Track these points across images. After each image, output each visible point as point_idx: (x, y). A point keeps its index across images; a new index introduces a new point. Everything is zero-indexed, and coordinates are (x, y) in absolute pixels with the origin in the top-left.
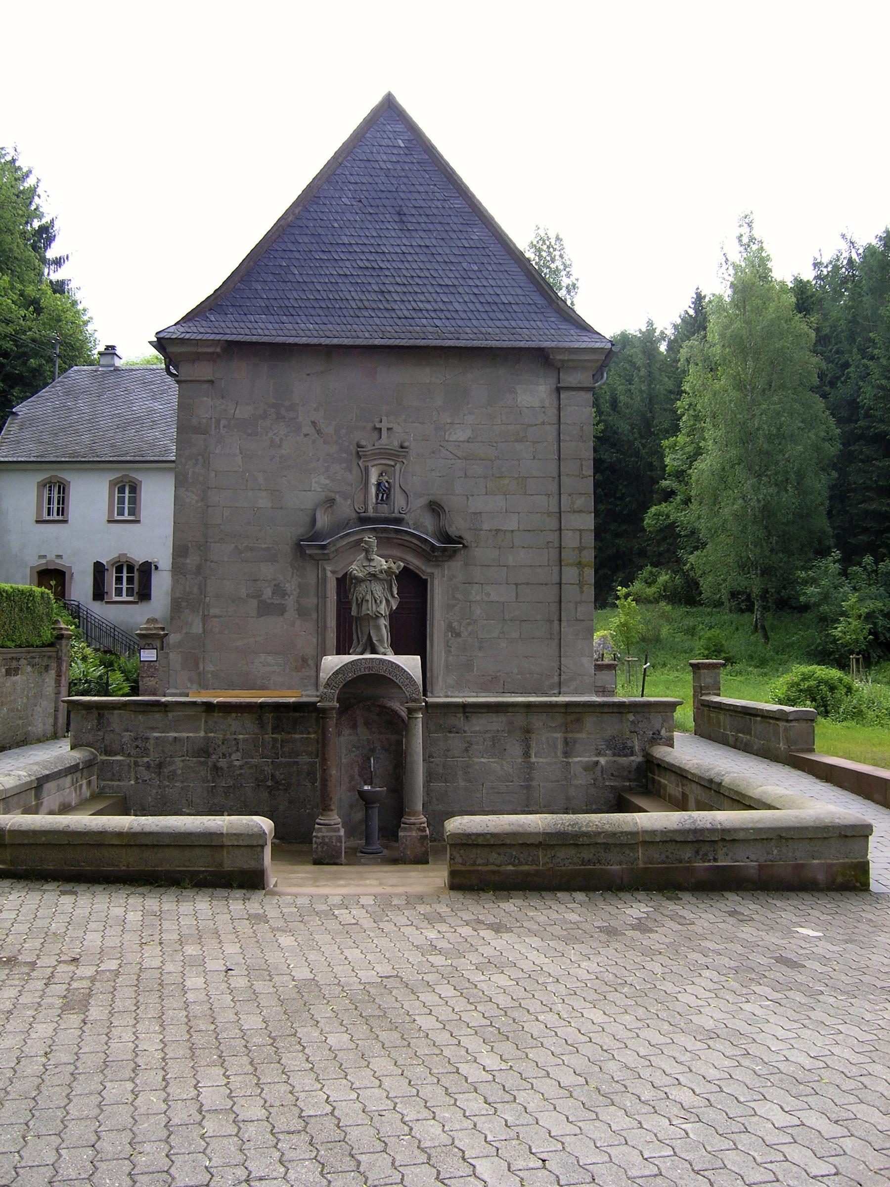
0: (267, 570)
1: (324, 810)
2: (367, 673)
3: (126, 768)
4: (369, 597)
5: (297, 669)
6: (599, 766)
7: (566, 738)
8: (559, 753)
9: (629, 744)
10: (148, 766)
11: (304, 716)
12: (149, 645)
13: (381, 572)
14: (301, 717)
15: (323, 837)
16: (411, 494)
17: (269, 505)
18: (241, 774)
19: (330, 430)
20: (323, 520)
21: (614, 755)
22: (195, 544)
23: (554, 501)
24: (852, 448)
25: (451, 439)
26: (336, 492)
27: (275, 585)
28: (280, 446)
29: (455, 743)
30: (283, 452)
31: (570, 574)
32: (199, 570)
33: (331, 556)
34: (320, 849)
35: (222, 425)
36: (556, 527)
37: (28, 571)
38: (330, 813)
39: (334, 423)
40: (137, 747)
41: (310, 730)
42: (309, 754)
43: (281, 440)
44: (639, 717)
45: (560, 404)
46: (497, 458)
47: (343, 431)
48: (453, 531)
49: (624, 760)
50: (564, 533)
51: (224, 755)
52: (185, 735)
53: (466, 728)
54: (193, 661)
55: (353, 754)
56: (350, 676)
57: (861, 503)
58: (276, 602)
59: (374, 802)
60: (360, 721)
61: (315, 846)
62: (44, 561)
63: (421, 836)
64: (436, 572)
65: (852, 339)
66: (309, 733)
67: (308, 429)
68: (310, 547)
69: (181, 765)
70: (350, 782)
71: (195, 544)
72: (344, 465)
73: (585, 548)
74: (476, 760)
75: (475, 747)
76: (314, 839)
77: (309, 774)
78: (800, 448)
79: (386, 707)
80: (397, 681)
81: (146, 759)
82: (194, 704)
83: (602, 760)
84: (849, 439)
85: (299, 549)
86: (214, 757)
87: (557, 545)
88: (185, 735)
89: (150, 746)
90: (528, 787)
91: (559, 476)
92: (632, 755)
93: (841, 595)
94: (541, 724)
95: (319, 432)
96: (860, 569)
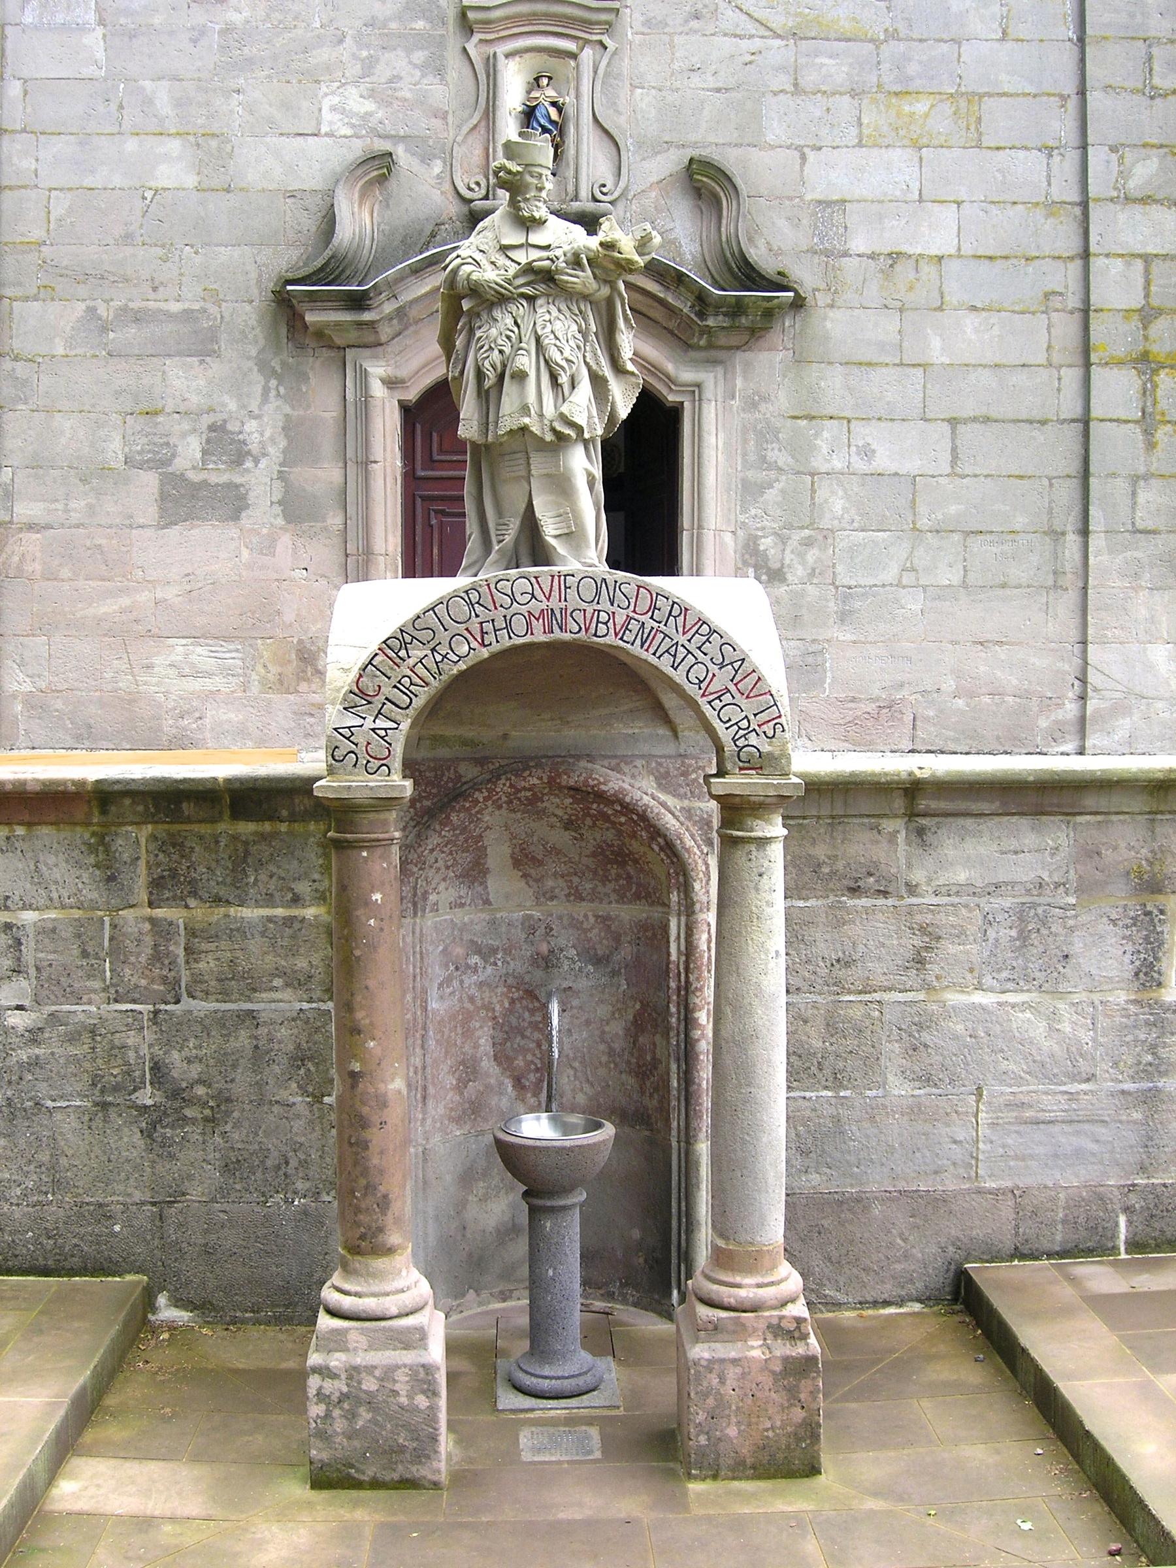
0: (185, 382)
1: (355, 1250)
2: (540, 637)
4: (526, 362)
5: (282, 685)
11: (275, 835)
13: (575, 262)
14: (263, 837)
15: (354, 1372)
17: (191, 181)
18: (35, 1063)
20: (357, 223)
23: (1066, 166)
27: (212, 428)
29: (876, 932)
31: (1116, 391)
33: (385, 331)
34: (339, 1425)
36: (1075, 246)
38: (380, 1263)
41: (303, 888)
42: (297, 982)
46: (893, 35)
48: (760, 256)
50: (1096, 264)
53: (918, 876)
55: (470, 980)
56: (465, 653)
58: (214, 479)
59: (567, 1190)
60: (498, 853)
61: (316, 1410)
63: (786, 1360)
64: (710, 379)
66: (296, 900)
68: (318, 306)
72: (419, 56)
73: (1160, 312)
74: (954, 998)
75: (953, 949)
76: (314, 1382)
77: (299, 1059)
79: (600, 796)
80: (678, 676)
85: (287, 309)
87: (1074, 302)
91: (1082, 93)
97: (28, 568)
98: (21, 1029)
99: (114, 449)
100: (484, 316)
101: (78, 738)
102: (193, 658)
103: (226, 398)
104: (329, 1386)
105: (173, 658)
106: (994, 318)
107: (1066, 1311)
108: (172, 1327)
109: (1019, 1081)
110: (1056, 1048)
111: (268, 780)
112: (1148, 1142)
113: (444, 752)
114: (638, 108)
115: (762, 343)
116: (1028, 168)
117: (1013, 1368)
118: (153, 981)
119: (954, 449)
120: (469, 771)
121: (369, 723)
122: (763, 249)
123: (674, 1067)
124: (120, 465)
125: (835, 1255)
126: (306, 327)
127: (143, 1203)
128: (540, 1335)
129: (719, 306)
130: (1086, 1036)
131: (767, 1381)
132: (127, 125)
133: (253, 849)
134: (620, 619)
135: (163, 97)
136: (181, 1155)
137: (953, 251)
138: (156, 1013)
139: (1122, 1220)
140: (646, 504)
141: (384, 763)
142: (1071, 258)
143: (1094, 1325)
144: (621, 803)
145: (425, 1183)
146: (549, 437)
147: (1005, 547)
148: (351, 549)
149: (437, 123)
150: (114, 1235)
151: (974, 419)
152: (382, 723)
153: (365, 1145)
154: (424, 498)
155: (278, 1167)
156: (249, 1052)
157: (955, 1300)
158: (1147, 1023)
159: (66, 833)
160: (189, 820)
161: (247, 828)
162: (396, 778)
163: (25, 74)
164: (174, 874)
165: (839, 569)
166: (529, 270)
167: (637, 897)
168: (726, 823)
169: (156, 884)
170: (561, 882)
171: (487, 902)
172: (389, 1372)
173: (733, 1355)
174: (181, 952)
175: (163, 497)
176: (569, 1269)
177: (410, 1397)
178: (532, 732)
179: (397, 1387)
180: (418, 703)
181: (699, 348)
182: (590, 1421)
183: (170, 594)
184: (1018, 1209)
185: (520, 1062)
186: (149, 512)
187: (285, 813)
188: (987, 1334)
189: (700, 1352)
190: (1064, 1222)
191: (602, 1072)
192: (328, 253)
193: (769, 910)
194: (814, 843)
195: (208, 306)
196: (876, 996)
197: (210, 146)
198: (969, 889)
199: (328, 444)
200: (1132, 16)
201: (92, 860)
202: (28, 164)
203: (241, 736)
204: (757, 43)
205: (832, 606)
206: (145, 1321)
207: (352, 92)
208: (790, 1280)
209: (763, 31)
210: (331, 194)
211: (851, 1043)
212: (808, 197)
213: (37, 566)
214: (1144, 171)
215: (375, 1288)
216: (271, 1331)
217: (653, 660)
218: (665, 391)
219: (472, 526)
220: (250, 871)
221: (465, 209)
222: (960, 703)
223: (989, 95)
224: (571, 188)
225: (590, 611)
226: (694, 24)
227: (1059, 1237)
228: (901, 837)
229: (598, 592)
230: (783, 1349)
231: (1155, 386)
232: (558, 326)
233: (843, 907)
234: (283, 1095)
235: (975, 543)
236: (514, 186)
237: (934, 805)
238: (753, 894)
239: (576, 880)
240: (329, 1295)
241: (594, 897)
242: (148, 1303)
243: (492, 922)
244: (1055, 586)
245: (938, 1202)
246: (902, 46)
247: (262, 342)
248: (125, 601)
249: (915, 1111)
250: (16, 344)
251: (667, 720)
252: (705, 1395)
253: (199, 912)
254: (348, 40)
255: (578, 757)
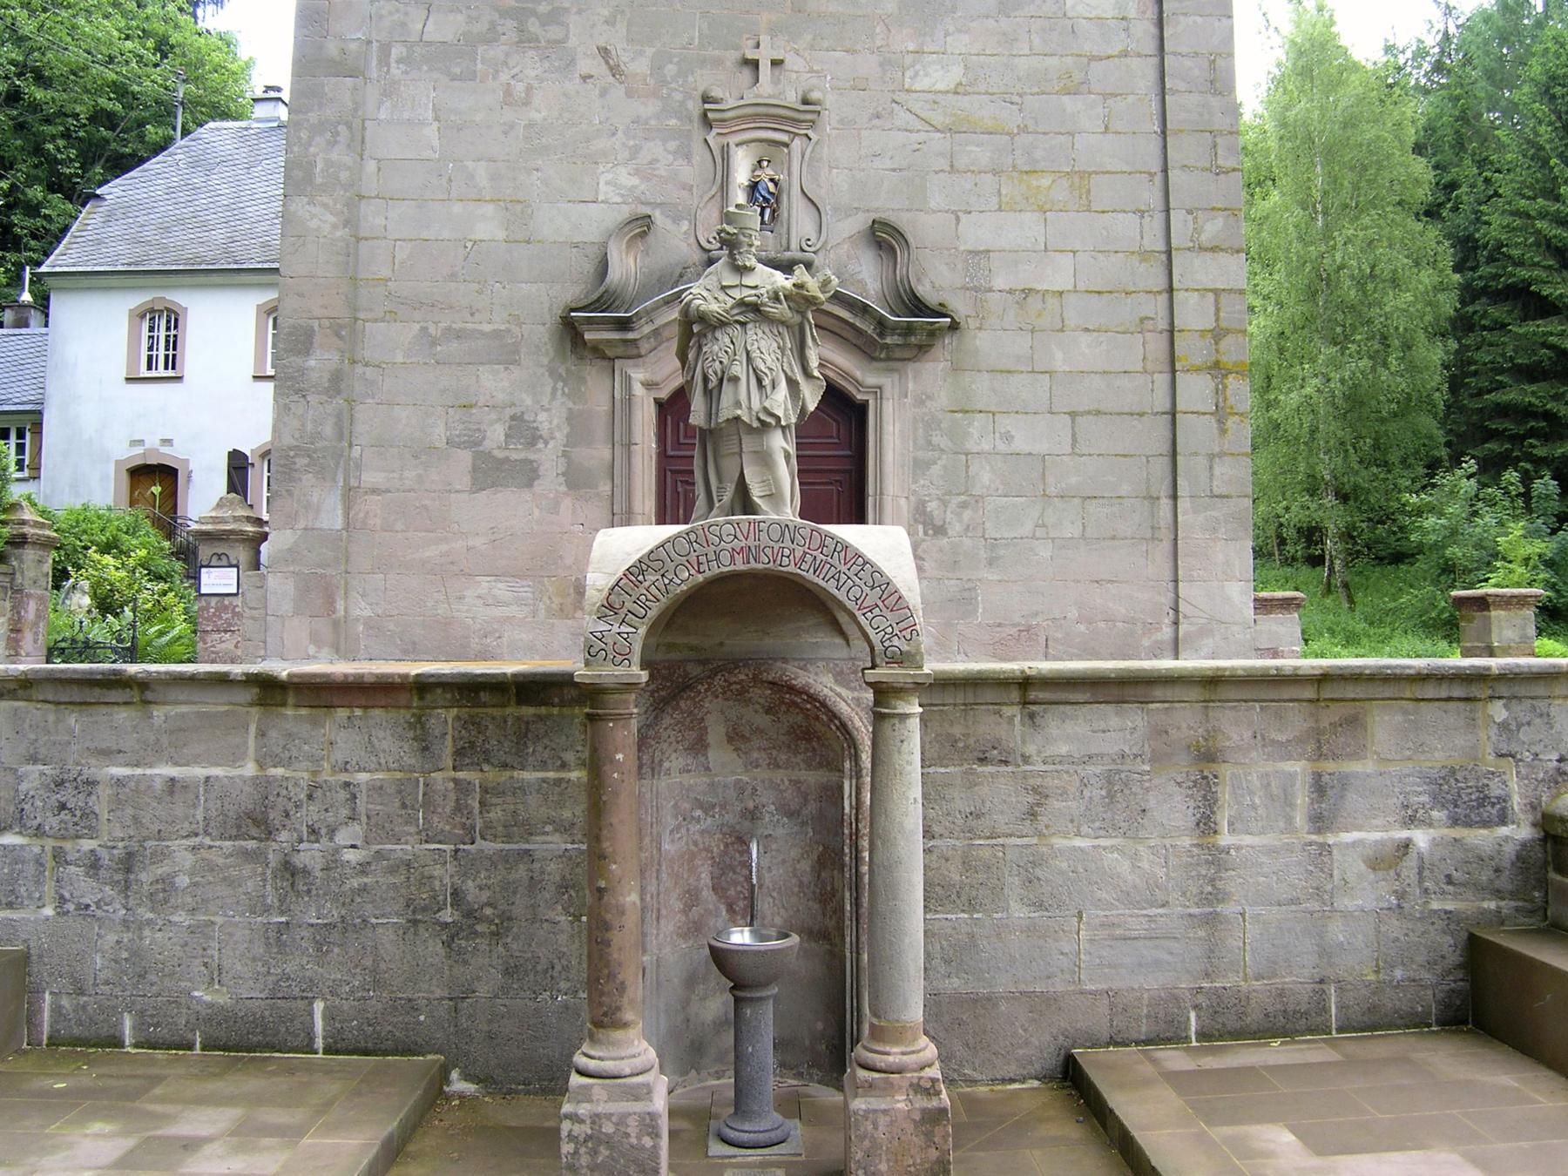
0: (494, 383)
1: (599, 1024)
2: (740, 566)
3: (31, 869)
4: (739, 369)
5: (562, 612)
6: (1413, 854)
7: (1318, 776)
8: (1300, 819)
9: (1495, 790)
10: (93, 865)
12: (219, 556)
13: (776, 298)
14: (540, 718)
15: (596, 1118)
16: (826, 209)
18: (364, 889)
19: (639, 67)
20: (625, 267)
21: (1455, 822)
22: (326, 323)
24: (1470, 309)
25: (917, 87)
26: (655, 205)
27: (513, 418)
28: (526, 103)
29: (999, 791)
30: (537, 116)
31: (1195, 390)
32: (336, 382)
33: (644, 347)
34: (585, 1160)
35: (394, 56)
36: (1162, 283)
37: (112, 467)
38: (618, 1034)
39: (650, 51)
40: (63, 806)
41: (569, 757)
43: (529, 88)
44: (1521, 711)
45: (1161, 12)
46: (1023, 129)
47: (671, 69)
48: (925, 291)
49: (1480, 838)
50: (1179, 296)
51: (313, 831)
52: (199, 772)
53: (1030, 749)
54: (321, 594)
56: (686, 579)
57: (1489, 392)
58: (514, 456)
60: (716, 732)
61: (567, 1148)
62: (139, 450)
63: (924, 1111)
64: (887, 382)
65: (1460, 145)
66: (564, 766)
67: (589, 64)
68: (592, 330)
69: (188, 860)
70: (686, 910)
71: (326, 323)
72: (672, 145)
73: (1227, 332)
74: (1059, 842)
76: (566, 1126)
77: (563, 887)
78: (1409, 296)
79: (792, 689)
81: (87, 845)
82: (223, 680)
83: (1421, 838)
84: (1469, 294)
85: (571, 332)
86: (283, 836)
87: (1163, 324)
88: (199, 772)
89: (101, 803)
90: (1212, 921)
91: (1165, 170)
92: (1503, 820)
93: (1478, 530)
94: (1248, 734)
95: (615, 70)
96: (1499, 493)
97: (371, 522)
98: (354, 863)
99: (439, 434)
100: (709, 336)
101: (406, 652)
102: (496, 592)
103: (524, 396)
104: (578, 1129)
105: (480, 591)
106: (1103, 337)
107: (1147, 1083)
108: (461, 1096)
109: (1110, 906)
110: (1138, 881)
111: (545, 675)
112: (1210, 954)
113: (675, 656)
114: (834, 184)
115: (928, 356)
116: (1126, 225)
117: (1104, 1126)
118: (454, 827)
119: (1074, 435)
120: (695, 670)
121: (615, 629)
122: (928, 286)
123: (847, 895)
124: (443, 445)
125: (971, 1042)
126: (585, 343)
127: (443, 999)
128: (742, 1102)
129: (895, 328)
130: (1161, 872)
131: (910, 1127)
132: (454, 194)
133: (532, 727)
134: (798, 554)
135: (481, 172)
136: (472, 962)
137: (1070, 287)
138: (457, 851)
139: (1193, 1015)
140: (840, 472)
141: (626, 657)
142: (1159, 293)
143: (1168, 1093)
144: (810, 696)
145: (658, 984)
146: (756, 424)
147: (1114, 509)
148: (617, 509)
149: (685, 194)
150: (420, 1023)
151: (1089, 413)
152: (625, 629)
153: (607, 943)
154: (673, 472)
155: (546, 971)
156: (526, 882)
157: (1065, 1078)
158: (1207, 862)
159: (392, 714)
160: (485, 706)
161: (528, 711)
162: (636, 669)
163: (379, 156)
164: (472, 744)
165: (988, 525)
166: (742, 303)
167: (820, 765)
168: (877, 703)
169: (459, 753)
170: (763, 754)
171: (708, 769)
172: (623, 1119)
173: (883, 1106)
174: (477, 805)
175: (475, 469)
176: (764, 1050)
177: (639, 1138)
178: (742, 641)
179: (629, 1130)
180: (652, 614)
181: (881, 360)
182: (778, 1165)
183: (478, 542)
184: (1112, 1006)
185: (732, 892)
186: (465, 481)
187: (556, 700)
188: (1088, 1103)
189: (859, 1104)
190: (1148, 1016)
191: (794, 899)
192: (602, 289)
193: (909, 768)
194: (952, 724)
195: (513, 327)
196: (1001, 841)
197: (516, 209)
198: (1069, 759)
199: (600, 427)
200: (1201, 115)
201: (411, 734)
202: (380, 221)
203: (525, 641)
204: (922, 136)
205: (983, 554)
206: (441, 1092)
207: (622, 171)
208: (928, 1049)
209: (928, 128)
210: (605, 245)
211: (981, 877)
212: (962, 248)
213: (378, 521)
214: (1213, 228)
215: (614, 1054)
216: (538, 1100)
217: (821, 583)
218: (854, 392)
219: (700, 489)
220: (529, 744)
221: (705, 256)
222: (1082, 627)
223: (1096, 173)
224: (784, 242)
225: (776, 547)
226: (876, 122)
227: (1144, 1029)
228: (1017, 720)
229: (783, 534)
230: (922, 1102)
231: (1225, 387)
232: (763, 343)
233: (971, 772)
234: (551, 915)
235: (1092, 506)
236: (730, 244)
237: (1042, 695)
238: (896, 756)
239: (775, 753)
240: (580, 1060)
241: (789, 765)
242: (445, 1078)
243: (712, 784)
244: (1153, 538)
245: (1050, 1001)
246: (1031, 137)
247: (552, 354)
248: (444, 547)
249: (1031, 929)
250: (367, 354)
251: (842, 633)
252: (862, 1138)
253: (492, 775)
254: (620, 133)
255: (775, 660)
